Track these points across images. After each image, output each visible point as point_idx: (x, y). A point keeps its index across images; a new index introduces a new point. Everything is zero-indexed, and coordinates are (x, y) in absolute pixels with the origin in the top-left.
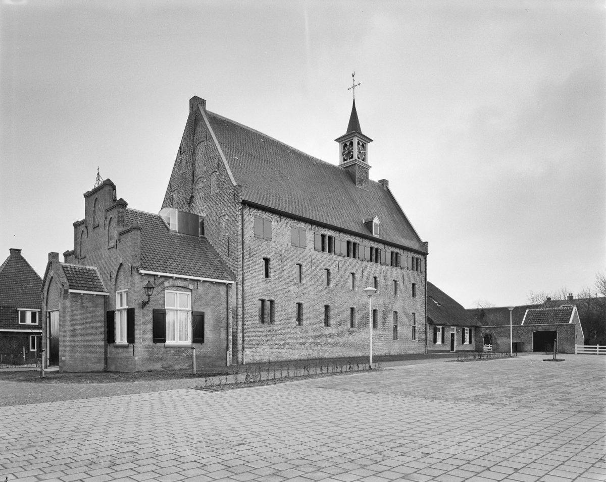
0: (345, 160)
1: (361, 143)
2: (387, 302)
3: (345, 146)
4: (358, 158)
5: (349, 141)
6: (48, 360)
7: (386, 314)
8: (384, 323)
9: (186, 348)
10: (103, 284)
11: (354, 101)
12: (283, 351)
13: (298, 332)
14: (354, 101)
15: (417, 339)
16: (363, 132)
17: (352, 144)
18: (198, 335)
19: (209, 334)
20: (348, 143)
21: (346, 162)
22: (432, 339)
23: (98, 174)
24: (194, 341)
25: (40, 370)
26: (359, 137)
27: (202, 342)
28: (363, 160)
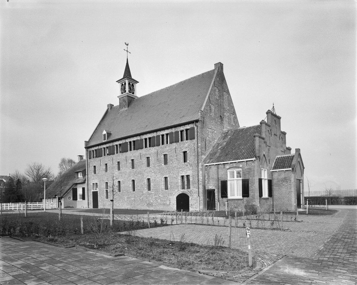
0: (122, 93)
1: (131, 84)
3: (122, 85)
4: (129, 92)
5: (124, 82)
6: (301, 193)
10: (281, 156)
11: (127, 59)
14: (127, 59)
16: (133, 77)
17: (125, 84)
18: (246, 192)
20: (124, 84)
21: (123, 94)
23: (273, 107)
24: (243, 196)
25: (214, 218)
26: (129, 80)
27: (248, 196)
28: (132, 93)
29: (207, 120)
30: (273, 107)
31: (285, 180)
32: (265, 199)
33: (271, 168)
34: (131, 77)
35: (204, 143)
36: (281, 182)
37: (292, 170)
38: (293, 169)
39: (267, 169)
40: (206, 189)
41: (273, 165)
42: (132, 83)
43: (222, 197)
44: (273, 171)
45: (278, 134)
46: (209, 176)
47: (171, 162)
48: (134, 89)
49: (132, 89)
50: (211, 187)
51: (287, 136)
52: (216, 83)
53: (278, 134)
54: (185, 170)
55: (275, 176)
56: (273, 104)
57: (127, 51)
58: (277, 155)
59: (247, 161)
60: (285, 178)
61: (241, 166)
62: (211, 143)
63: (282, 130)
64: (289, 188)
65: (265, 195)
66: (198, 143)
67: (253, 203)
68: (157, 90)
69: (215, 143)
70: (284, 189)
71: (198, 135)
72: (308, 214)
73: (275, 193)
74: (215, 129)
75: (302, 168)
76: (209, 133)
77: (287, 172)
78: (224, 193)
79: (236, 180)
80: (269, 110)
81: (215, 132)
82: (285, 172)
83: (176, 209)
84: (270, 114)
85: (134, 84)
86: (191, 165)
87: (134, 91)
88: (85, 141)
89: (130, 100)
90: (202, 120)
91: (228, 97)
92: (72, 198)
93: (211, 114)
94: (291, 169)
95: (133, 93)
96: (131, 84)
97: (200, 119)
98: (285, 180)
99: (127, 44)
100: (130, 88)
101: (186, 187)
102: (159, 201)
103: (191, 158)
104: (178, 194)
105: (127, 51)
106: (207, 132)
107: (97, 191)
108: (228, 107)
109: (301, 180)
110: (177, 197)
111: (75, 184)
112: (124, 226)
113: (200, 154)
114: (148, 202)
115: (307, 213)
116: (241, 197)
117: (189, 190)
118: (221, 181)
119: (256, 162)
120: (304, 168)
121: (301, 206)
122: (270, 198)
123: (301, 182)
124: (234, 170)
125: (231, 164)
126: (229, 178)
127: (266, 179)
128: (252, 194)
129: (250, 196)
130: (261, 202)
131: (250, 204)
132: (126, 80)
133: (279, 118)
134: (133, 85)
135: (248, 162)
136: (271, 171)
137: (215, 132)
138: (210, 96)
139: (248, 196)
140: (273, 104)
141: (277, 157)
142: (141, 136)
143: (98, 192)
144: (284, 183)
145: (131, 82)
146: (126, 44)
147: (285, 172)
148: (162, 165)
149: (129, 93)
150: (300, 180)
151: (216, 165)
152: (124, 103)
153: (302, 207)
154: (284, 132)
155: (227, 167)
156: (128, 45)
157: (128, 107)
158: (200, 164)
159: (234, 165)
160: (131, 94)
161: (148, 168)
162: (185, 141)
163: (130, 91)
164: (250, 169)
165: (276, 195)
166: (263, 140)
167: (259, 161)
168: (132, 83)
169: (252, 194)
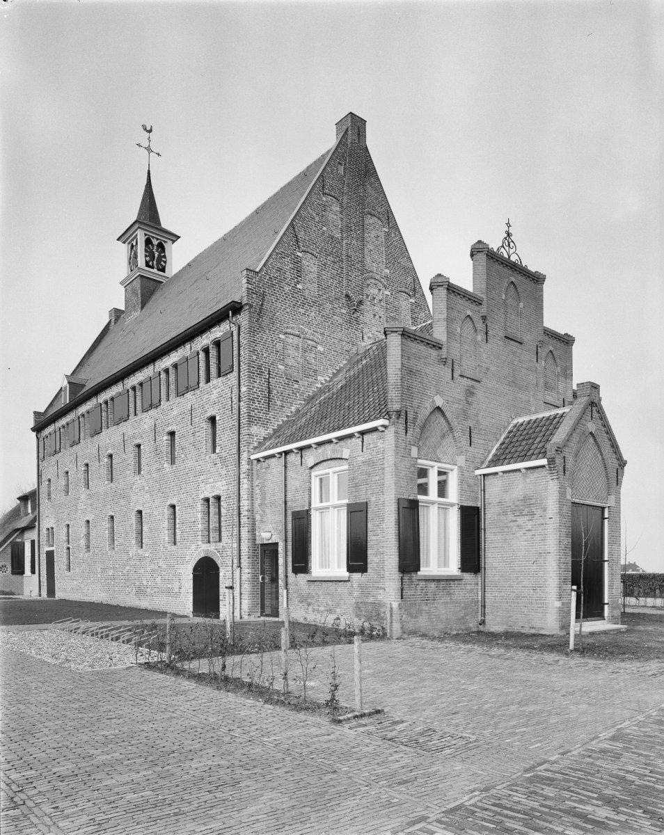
1: (155, 242)
3: (132, 246)
4: (147, 265)
6: (606, 559)
11: (149, 171)
14: (149, 171)
16: (165, 224)
23: (509, 234)
24: (351, 569)
27: (363, 569)
29: (279, 307)
30: (509, 234)
31: (528, 506)
32: (439, 581)
33: (482, 463)
34: (160, 224)
35: (259, 383)
36: (511, 517)
37: (549, 464)
38: (551, 461)
39: (455, 468)
40: (258, 542)
41: (494, 451)
42: (157, 239)
43: (296, 571)
44: (484, 475)
45: (530, 338)
46: (263, 499)
47: (183, 456)
48: (165, 257)
49: (156, 255)
50: (265, 536)
51: (576, 348)
52: (328, 182)
53: (530, 338)
54: (212, 480)
55: (494, 489)
56: (508, 225)
57: (149, 149)
58: (518, 415)
59: (363, 433)
60: (526, 499)
61: (346, 454)
62: (296, 386)
63: (554, 319)
64: (538, 538)
65: (324, 564)
66: (239, 385)
67: (380, 597)
68: (206, 247)
69: (319, 386)
70: (520, 544)
71: (239, 354)
72: (576, 650)
73: (492, 555)
74: (318, 337)
75: (612, 462)
76: (291, 352)
77: (533, 476)
78: (301, 562)
79: (335, 507)
80: (480, 242)
81: (320, 348)
82: (525, 476)
83: (191, 609)
84: (482, 257)
85: (165, 242)
86: (223, 460)
87: (165, 262)
88: (35, 413)
89: (146, 289)
90: (256, 301)
91: (388, 235)
92: (9, 569)
93: (299, 286)
94: (544, 462)
95: (163, 270)
96: (155, 242)
97: (245, 301)
98: (528, 506)
99: (148, 128)
100: (150, 254)
101: (214, 535)
102: (158, 580)
103: (226, 437)
104: (197, 559)
105: (149, 149)
106: (279, 346)
107: (53, 551)
108: (387, 268)
109: (606, 510)
110: (195, 569)
111: (17, 530)
112: (372, 631)
113: (244, 421)
114: (137, 583)
115: (572, 646)
116: (343, 572)
117: (220, 545)
118: (293, 512)
119: (390, 434)
120: (622, 464)
121: (603, 609)
122: (468, 577)
123: (606, 515)
124: (327, 471)
125: (321, 450)
126: (316, 503)
127: (452, 505)
128: (376, 560)
129: (369, 570)
130: (407, 592)
131: (371, 600)
132: (139, 232)
133: (537, 279)
134: (161, 247)
135: (366, 437)
136: (478, 472)
137: (320, 348)
138: (298, 224)
139: (363, 569)
140: (508, 225)
141: (515, 422)
142: (126, 381)
143: (55, 554)
144: (521, 520)
145: (153, 237)
146: (145, 129)
147: (525, 476)
148: (166, 465)
149: (147, 269)
150: (603, 508)
151: (280, 453)
152: (134, 298)
153: (606, 614)
154: (566, 334)
155: (310, 459)
156: (150, 131)
157: (142, 308)
158: (244, 456)
159: (328, 451)
160: (155, 271)
161: (137, 478)
162: (215, 381)
163: (151, 264)
164: (369, 463)
165: (495, 565)
166: (434, 353)
167: (402, 431)
168: (157, 239)
169: (376, 560)
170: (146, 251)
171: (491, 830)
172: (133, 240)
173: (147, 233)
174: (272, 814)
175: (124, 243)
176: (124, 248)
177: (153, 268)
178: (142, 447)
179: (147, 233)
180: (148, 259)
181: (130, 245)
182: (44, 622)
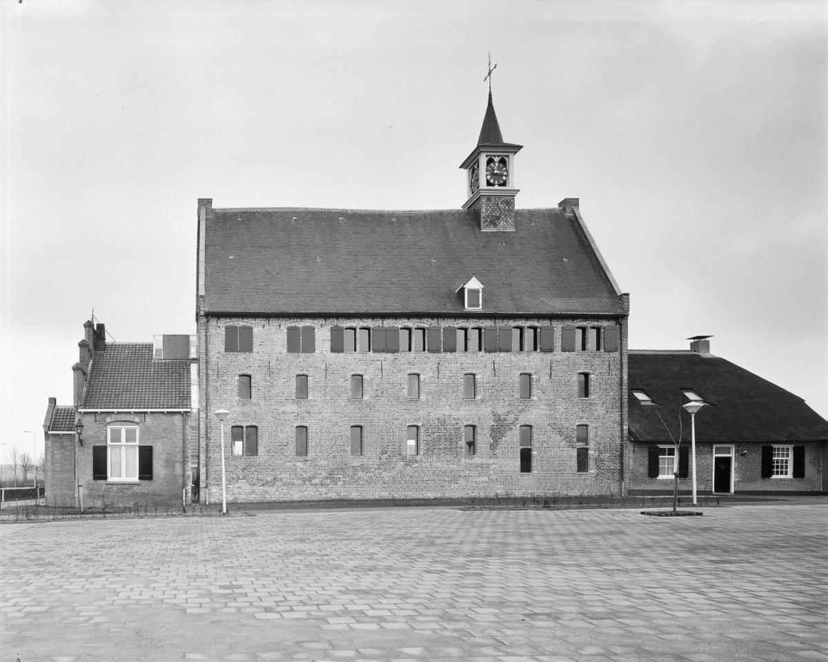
2: (501, 411)
3: (474, 169)
7: (498, 431)
8: (493, 447)
9: (132, 485)
11: (490, 95)
12: (272, 490)
13: (299, 464)
14: (490, 95)
15: (592, 471)
16: (507, 138)
19: (159, 468)
22: (643, 470)
27: (150, 478)
42: (499, 156)
96: (497, 159)
145: (495, 156)
149: (490, 188)
160: (496, 187)
170: (487, 170)
171: (372, 657)
172: (474, 164)
173: (488, 154)
174: (797, 549)
175: (466, 168)
176: (465, 173)
177: (493, 185)
178: (422, 377)
179: (488, 154)
180: (489, 177)
181: (471, 170)
182: (254, 213)
